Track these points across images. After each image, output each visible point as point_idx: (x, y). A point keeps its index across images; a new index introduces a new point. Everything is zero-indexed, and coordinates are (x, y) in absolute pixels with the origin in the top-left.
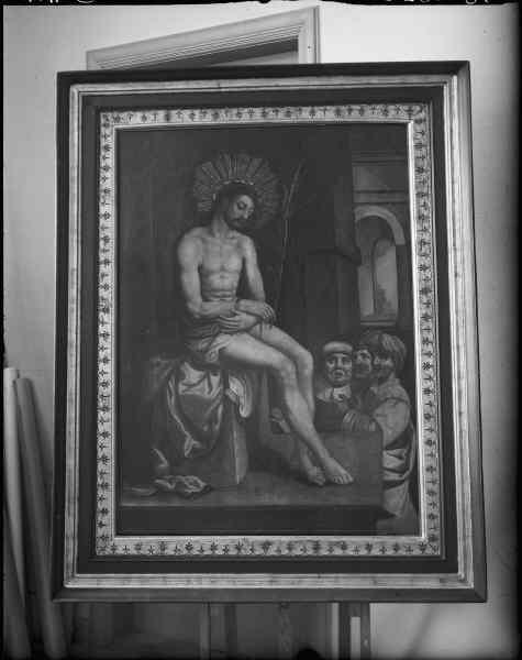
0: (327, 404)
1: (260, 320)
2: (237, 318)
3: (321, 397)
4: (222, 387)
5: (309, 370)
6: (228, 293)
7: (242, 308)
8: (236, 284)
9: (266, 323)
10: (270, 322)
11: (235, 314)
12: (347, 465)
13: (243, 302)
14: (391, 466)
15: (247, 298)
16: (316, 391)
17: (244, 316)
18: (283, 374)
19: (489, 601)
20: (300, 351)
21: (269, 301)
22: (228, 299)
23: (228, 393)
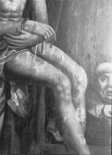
0: (99, 119)
1: (42, 39)
2: (22, 36)
3: (92, 112)
4: (4, 98)
5: (82, 89)
6: (16, 14)
7: (26, 28)
8: (23, 7)
9: (47, 43)
10: (50, 42)
11: (21, 33)
12: (19, 124)
13: (30, 23)
14: (105, 108)
15: (31, 19)
16: (88, 107)
17: (28, 35)
18: (59, 88)
19: (108, 112)
20: (72, 66)
21: (51, 21)
22: (16, 19)
23: (9, 104)
